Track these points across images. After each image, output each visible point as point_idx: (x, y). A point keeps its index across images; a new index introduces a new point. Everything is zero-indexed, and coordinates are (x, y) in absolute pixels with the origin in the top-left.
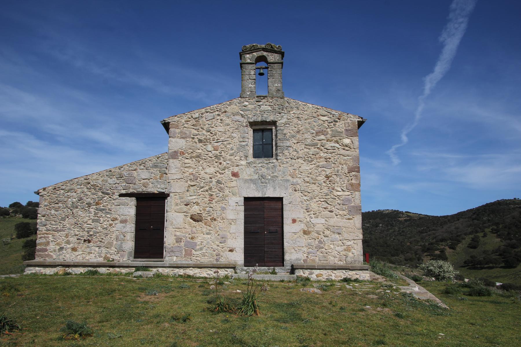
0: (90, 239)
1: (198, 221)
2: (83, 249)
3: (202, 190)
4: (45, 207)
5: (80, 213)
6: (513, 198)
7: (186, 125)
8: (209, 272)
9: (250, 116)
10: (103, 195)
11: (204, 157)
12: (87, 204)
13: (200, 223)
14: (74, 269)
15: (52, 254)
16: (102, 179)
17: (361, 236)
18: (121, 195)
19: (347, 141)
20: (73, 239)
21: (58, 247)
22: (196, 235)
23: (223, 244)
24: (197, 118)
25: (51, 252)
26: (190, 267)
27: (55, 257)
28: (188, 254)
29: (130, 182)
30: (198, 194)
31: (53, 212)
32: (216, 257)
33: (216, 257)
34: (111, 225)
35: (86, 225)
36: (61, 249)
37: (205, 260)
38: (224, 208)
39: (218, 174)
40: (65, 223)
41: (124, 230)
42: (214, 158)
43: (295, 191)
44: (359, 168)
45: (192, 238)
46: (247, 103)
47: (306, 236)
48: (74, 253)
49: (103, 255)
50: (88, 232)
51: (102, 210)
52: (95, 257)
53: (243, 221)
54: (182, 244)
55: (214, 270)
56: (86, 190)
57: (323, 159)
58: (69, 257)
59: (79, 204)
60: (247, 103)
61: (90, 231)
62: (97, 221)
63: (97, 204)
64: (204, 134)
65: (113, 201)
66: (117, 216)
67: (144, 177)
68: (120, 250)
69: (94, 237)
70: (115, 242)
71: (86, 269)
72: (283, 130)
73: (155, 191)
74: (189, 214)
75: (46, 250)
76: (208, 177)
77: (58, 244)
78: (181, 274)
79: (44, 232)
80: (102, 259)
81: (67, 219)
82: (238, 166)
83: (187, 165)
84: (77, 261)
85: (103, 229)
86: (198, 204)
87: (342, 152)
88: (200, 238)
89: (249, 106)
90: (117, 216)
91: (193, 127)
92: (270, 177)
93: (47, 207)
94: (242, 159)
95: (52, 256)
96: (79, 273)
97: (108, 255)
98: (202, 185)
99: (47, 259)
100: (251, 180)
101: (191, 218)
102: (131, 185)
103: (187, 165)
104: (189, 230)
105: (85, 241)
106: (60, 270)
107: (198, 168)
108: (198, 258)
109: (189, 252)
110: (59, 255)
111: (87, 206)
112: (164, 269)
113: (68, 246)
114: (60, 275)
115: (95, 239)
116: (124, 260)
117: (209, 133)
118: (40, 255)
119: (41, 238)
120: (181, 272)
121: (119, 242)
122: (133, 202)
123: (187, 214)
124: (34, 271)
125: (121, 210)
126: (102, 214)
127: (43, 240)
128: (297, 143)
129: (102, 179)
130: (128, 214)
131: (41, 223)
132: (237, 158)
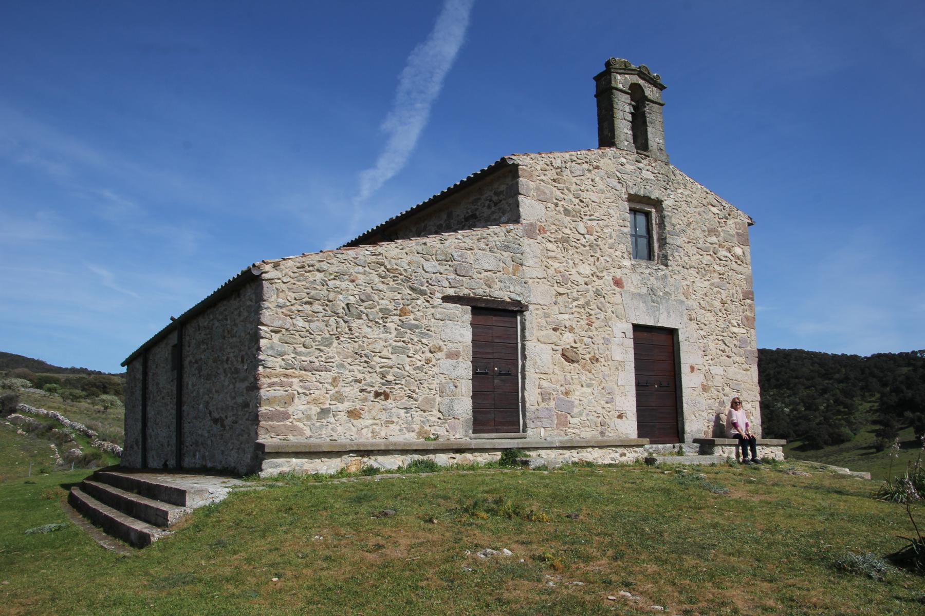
0: (388, 391)
1: (573, 361)
2: (374, 413)
3: (575, 304)
4: (279, 310)
5: (365, 330)
6: (910, 351)
7: (542, 177)
8: (614, 455)
9: (631, 184)
10: (414, 295)
11: (574, 244)
12: (381, 310)
13: (576, 365)
14: (380, 459)
15: (300, 425)
16: (409, 258)
17: (759, 398)
18: (446, 299)
19: (738, 251)
20: (351, 391)
21: (315, 410)
22: (572, 387)
23: (609, 405)
24: (559, 168)
25: (299, 420)
26: (588, 447)
27: (308, 434)
28: (563, 423)
29: (463, 273)
30: (570, 311)
31: (300, 322)
32: (600, 428)
33: (600, 428)
34: (428, 361)
35: (377, 359)
36: (324, 412)
37: (588, 434)
38: (608, 340)
39: (595, 279)
40: (332, 351)
41: (453, 375)
42: (588, 248)
43: (691, 320)
44: (752, 293)
45: (567, 393)
46: (624, 161)
47: (706, 394)
48: (355, 422)
49: (416, 427)
50: (383, 376)
51: (412, 328)
52: (400, 430)
53: (633, 365)
54: (552, 404)
55: (620, 450)
56: (377, 280)
57: (716, 275)
58: (362, 432)
59: (362, 308)
60: (624, 161)
61: (388, 373)
62: (403, 351)
63: (403, 313)
64: (570, 201)
65: (433, 310)
66: (441, 343)
67: (487, 267)
68: (447, 415)
69: (397, 387)
70: (438, 399)
71: (408, 459)
72: (670, 218)
73: (505, 296)
74: (560, 348)
75: (286, 416)
76: (581, 280)
77: (316, 402)
78: (576, 460)
79: (279, 370)
80: (413, 435)
81: (335, 343)
82: (620, 267)
83: (550, 254)
84: (362, 440)
85: (414, 369)
86: (571, 330)
87: (735, 266)
88: (577, 393)
89: (627, 166)
90: (441, 343)
91: (552, 182)
92: (661, 294)
93: (284, 310)
94: (625, 256)
95: (301, 433)
96: (395, 467)
97: (427, 428)
98: (575, 294)
99: (290, 437)
100: (639, 294)
101: (563, 355)
102: (464, 279)
103: (550, 254)
104: (561, 378)
105: (377, 395)
106: (353, 464)
107: (567, 262)
108: (576, 431)
109: (563, 419)
110: (320, 429)
111: (381, 315)
112: (549, 451)
113: (341, 406)
114: (356, 475)
115: (397, 391)
116: (458, 436)
117: (578, 201)
118: (272, 427)
119: (271, 385)
120: (574, 456)
121: (447, 400)
122: (464, 314)
123: (557, 348)
124: (286, 469)
125: (448, 331)
126: (412, 337)
127: (280, 392)
128: (689, 242)
129: (409, 258)
130: (461, 340)
131: (272, 348)
132: (618, 253)
